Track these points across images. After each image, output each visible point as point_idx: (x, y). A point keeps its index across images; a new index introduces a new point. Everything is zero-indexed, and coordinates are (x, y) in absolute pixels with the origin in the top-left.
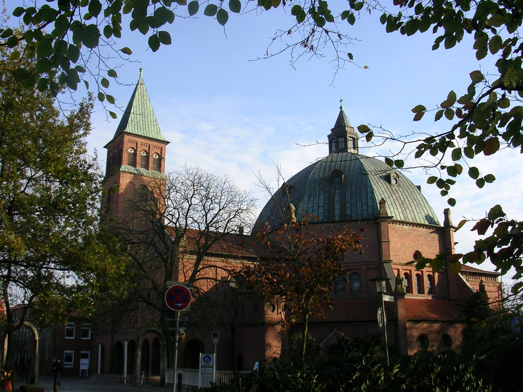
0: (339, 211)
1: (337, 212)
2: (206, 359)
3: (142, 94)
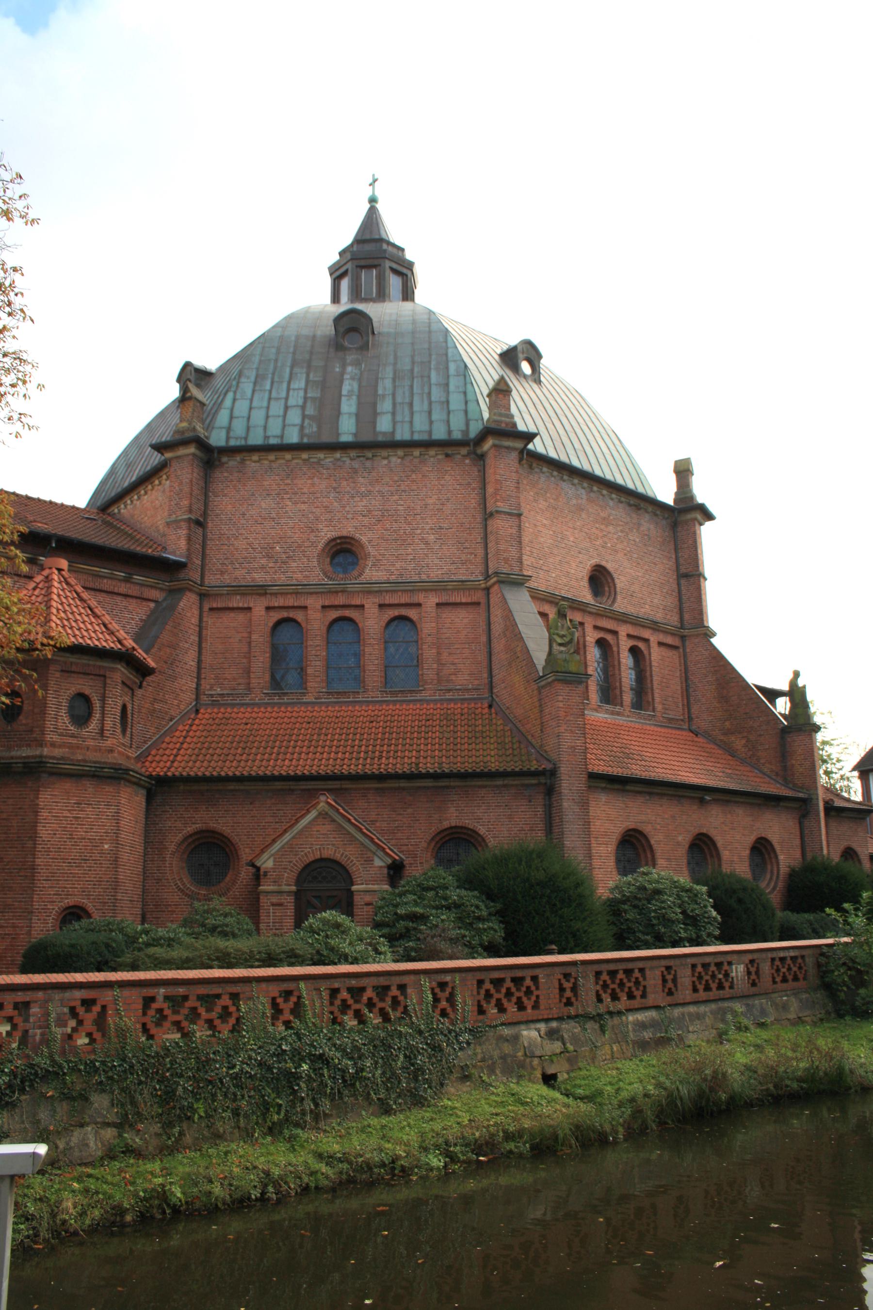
0: (353, 420)
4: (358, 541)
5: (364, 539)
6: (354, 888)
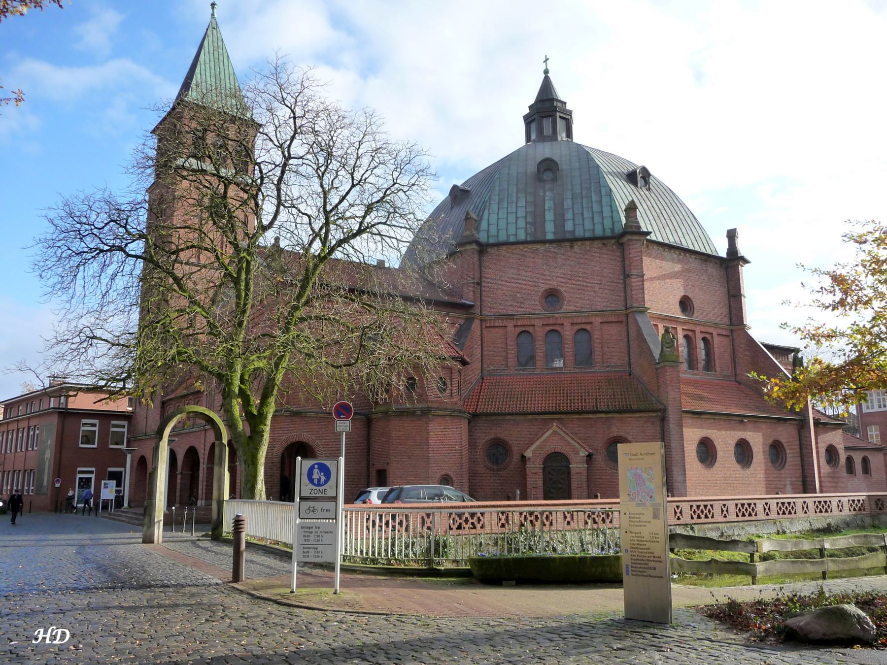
1: (550, 227)
2: (316, 476)
3: (215, 44)
4: (559, 291)
5: (562, 290)
6: (571, 466)
